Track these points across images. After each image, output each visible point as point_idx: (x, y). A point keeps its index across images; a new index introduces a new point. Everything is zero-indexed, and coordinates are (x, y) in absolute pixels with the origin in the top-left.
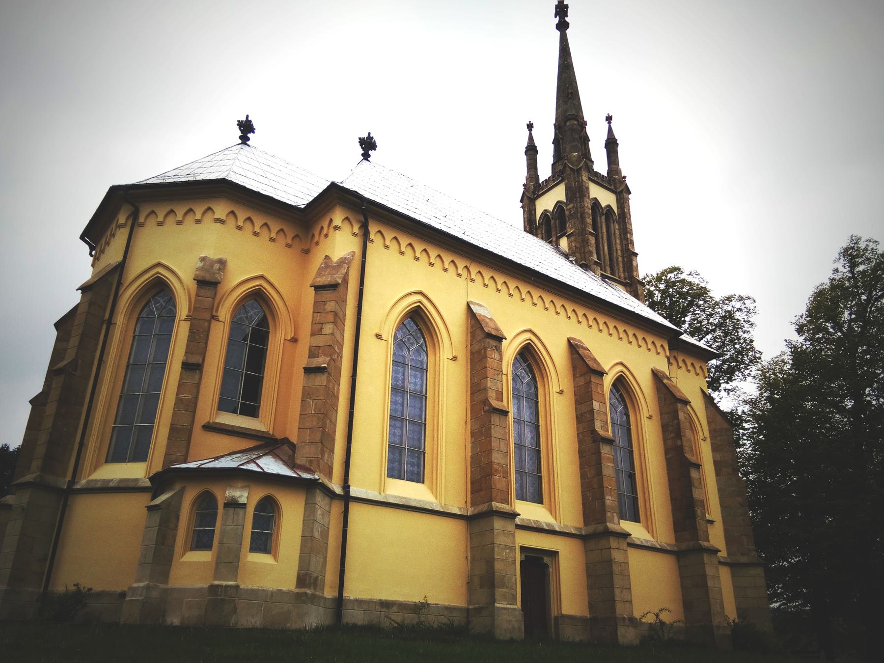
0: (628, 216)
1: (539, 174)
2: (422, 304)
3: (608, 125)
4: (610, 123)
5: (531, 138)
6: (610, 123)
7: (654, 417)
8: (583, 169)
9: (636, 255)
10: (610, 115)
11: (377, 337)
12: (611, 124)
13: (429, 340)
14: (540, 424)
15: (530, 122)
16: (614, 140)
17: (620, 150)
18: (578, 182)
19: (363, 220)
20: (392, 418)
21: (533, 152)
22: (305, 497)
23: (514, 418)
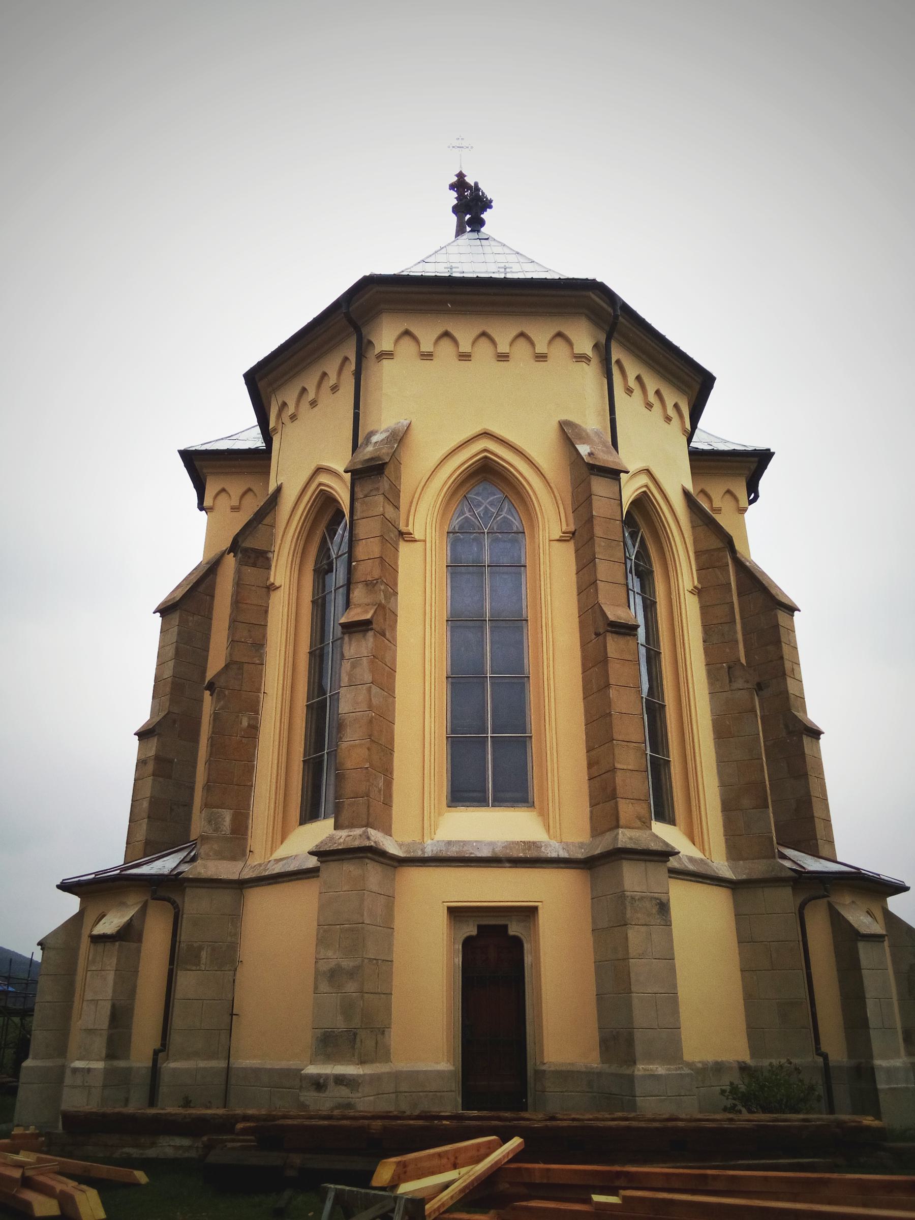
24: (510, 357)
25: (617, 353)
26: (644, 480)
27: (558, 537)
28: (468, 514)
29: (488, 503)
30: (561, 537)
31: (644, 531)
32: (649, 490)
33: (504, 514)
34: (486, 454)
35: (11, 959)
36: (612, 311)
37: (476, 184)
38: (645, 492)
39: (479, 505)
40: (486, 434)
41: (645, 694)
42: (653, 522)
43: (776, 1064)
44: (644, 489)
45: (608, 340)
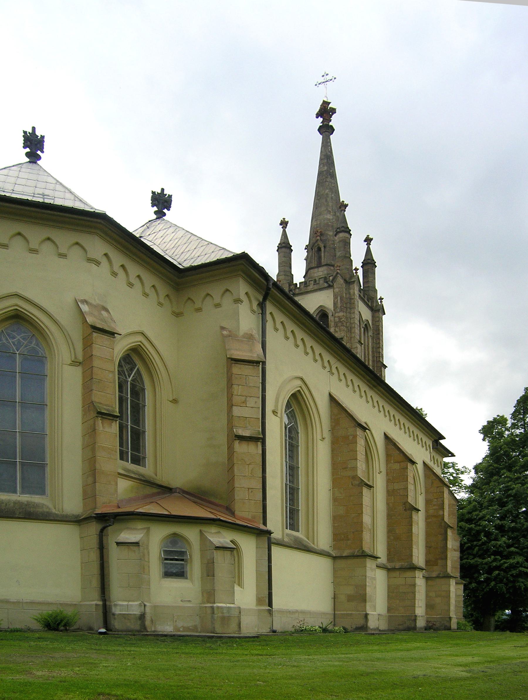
0: (381, 334)
1: (292, 273)
2: (302, 389)
3: (367, 246)
4: (369, 244)
5: (284, 234)
6: (369, 244)
7: (154, 476)
8: (355, 283)
9: (385, 367)
10: (286, 220)
11: (274, 413)
12: (370, 246)
13: (300, 418)
14: (300, 487)
15: (163, 190)
16: (373, 262)
17: (378, 271)
18: (350, 293)
19: (261, 300)
20: (42, 467)
21: (288, 251)
22: (255, 540)
23: (374, 487)
24: (100, 265)
25: (270, 308)
26: (299, 383)
27: (69, 364)
28: (5, 341)
29: (21, 337)
30: (70, 363)
31: (139, 365)
32: (302, 389)
33: (32, 345)
34: (16, 301)
35: (83, 500)
36: (266, 284)
37: (42, 137)
38: (299, 391)
39: (14, 338)
40: (143, 334)
41: (135, 511)
42: (142, 355)
43: (517, 556)
44: (299, 389)
45: (265, 299)
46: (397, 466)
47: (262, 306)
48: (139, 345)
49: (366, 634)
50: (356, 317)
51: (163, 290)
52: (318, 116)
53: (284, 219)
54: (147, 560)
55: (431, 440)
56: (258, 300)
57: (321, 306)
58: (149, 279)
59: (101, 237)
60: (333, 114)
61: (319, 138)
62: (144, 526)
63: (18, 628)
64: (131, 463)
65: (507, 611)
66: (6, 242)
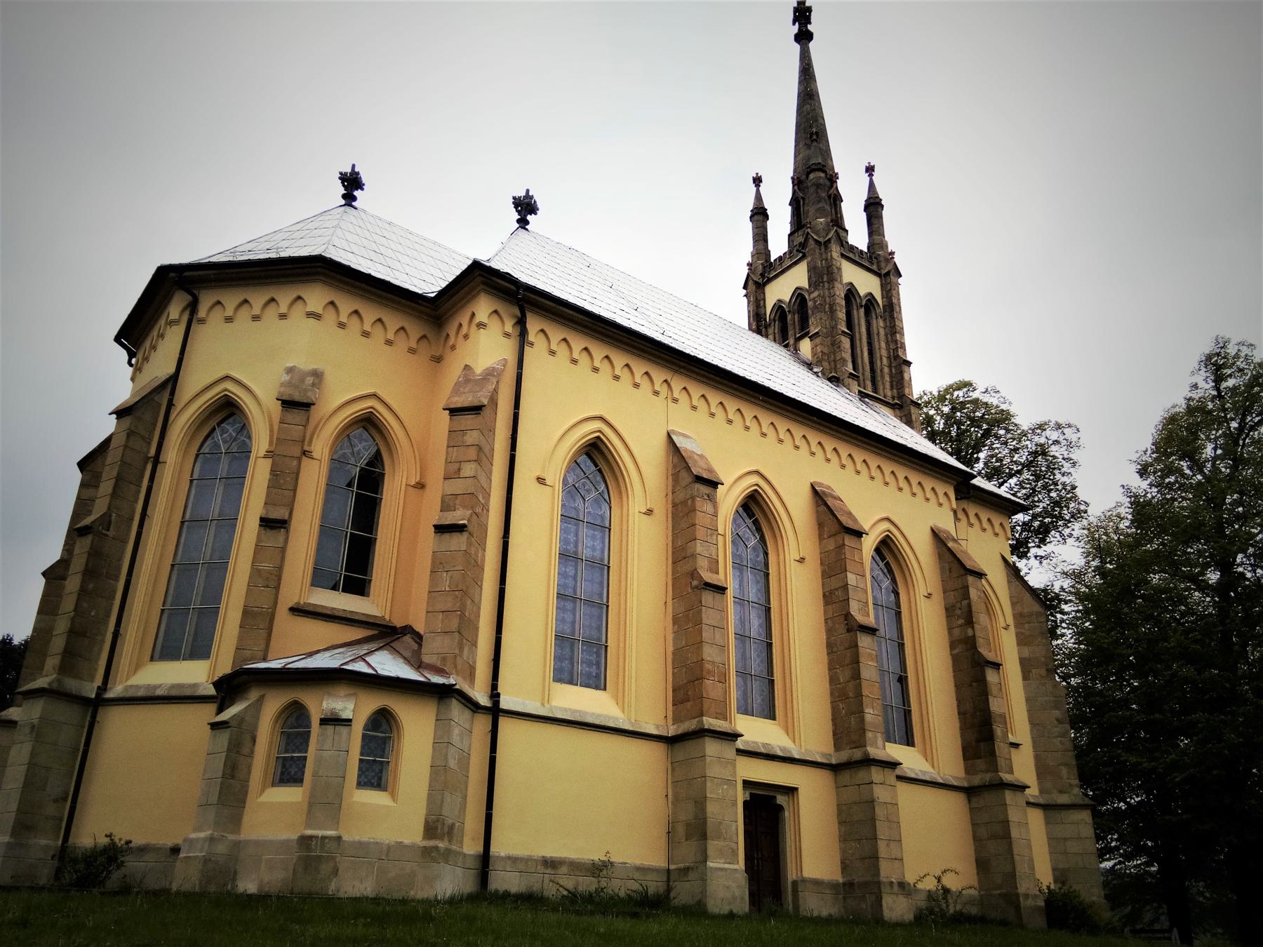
1: (769, 248)
2: (603, 434)
4: (871, 175)
6: (871, 175)
9: (909, 364)
10: (872, 164)
17: (886, 214)
46: (831, 545)
47: (521, 323)
48: (371, 412)
49: (102, 894)
50: (838, 293)
51: (415, 329)
52: (794, 24)
53: (869, 163)
54: (245, 751)
55: (951, 484)
56: (515, 316)
57: (797, 288)
58: (394, 321)
59: (324, 282)
60: (810, 14)
61: (797, 47)
62: (352, 692)
63: (596, 858)
64: (343, 591)
65: (1150, 844)
66: (320, 311)
